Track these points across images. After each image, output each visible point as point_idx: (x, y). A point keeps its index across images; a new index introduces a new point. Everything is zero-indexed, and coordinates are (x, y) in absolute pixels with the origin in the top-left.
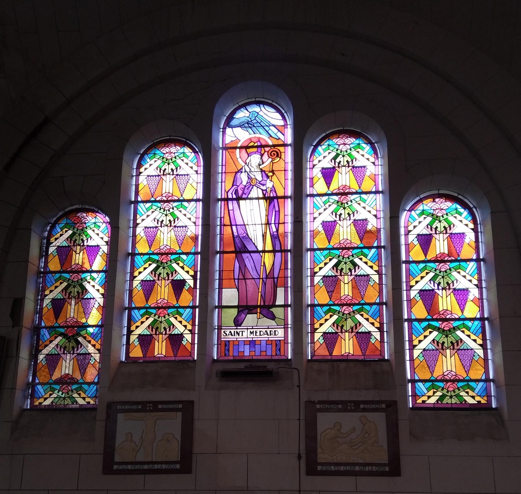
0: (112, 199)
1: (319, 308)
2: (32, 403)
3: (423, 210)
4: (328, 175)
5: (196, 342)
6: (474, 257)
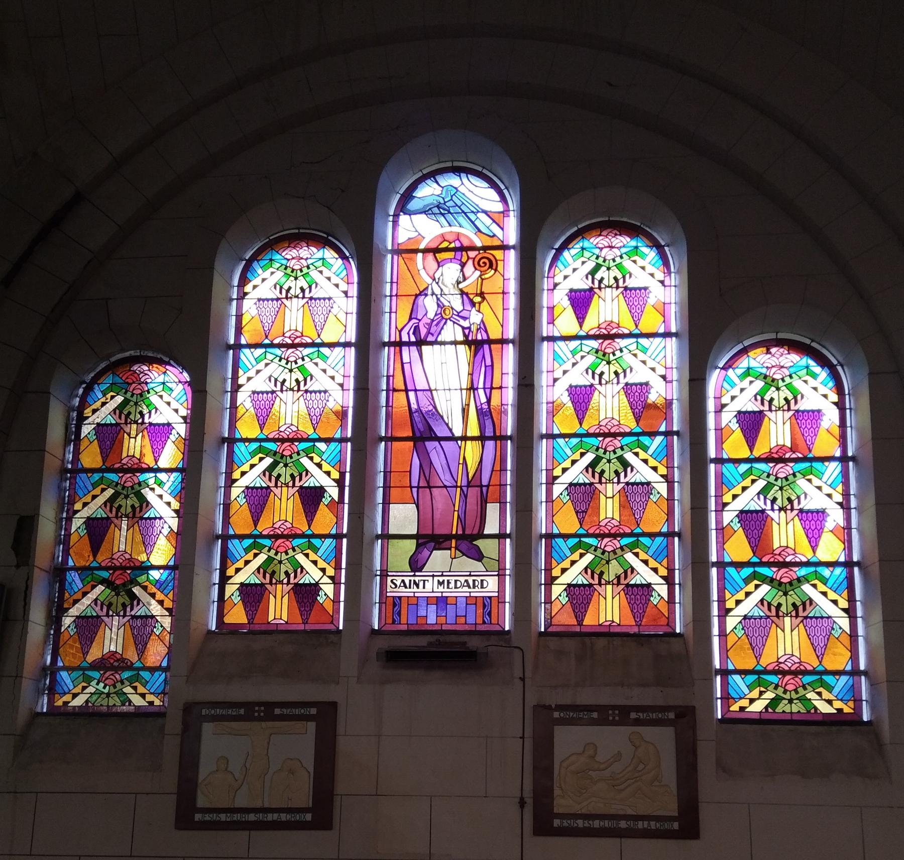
0: (194, 341)
1: (560, 541)
2: (51, 702)
3: (749, 368)
4: (581, 302)
5: (342, 598)
6: (838, 454)
